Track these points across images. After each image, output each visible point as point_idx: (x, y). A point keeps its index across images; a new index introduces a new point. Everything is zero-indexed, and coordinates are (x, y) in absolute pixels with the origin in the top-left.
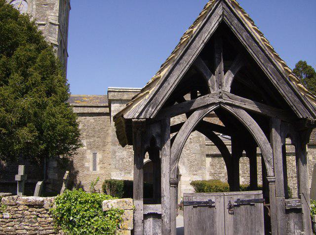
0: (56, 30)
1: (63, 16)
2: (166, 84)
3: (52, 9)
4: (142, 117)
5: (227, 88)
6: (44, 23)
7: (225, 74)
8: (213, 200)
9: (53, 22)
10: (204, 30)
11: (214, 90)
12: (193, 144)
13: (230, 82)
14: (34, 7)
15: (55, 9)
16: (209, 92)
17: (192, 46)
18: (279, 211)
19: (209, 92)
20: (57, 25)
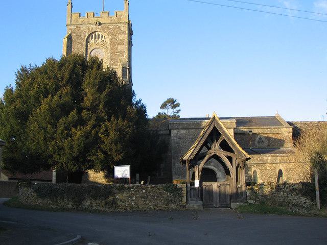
14: (109, 54)
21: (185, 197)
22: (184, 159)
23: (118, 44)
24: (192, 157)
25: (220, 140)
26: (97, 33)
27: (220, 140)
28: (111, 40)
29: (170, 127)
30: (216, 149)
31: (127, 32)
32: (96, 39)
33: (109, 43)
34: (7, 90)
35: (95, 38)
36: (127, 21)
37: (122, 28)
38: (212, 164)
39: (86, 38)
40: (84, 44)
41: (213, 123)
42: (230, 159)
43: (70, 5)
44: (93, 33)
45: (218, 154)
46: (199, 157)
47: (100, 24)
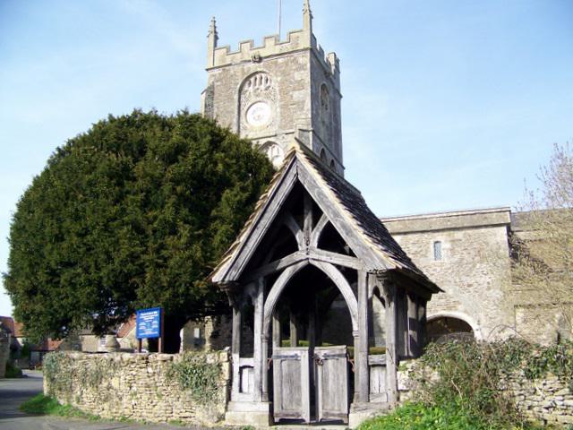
0: (308, 138)
1: (325, 116)
2: (246, 248)
3: (302, 109)
4: (227, 279)
5: (314, 243)
6: (291, 131)
7: (313, 227)
8: (299, 355)
9: (305, 128)
10: (279, 192)
11: (302, 247)
12: (492, 291)
13: (317, 237)
14: (278, 110)
15: (306, 108)
16: (297, 250)
17: (268, 210)
18: (361, 368)
19: (297, 250)
20: (309, 131)
21: (224, 389)
22: (213, 280)
23: (294, 90)
24: (234, 275)
25: (321, 225)
26: (258, 76)
27: (321, 225)
28: (282, 83)
29: (494, 250)
30: (308, 250)
31: (309, 65)
32: (257, 87)
33: (277, 89)
34: (35, 180)
35: (255, 85)
36: (308, 45)
37: (301, 60)
38: (460, 307)
39: (239, 86)
40: (236, 97)
41: (293, 171)
42: (351, 276)
43: (212, 36)
44: (257, 73)
45: (316, 264)
46: (259, 269)
47: (261, 59)
